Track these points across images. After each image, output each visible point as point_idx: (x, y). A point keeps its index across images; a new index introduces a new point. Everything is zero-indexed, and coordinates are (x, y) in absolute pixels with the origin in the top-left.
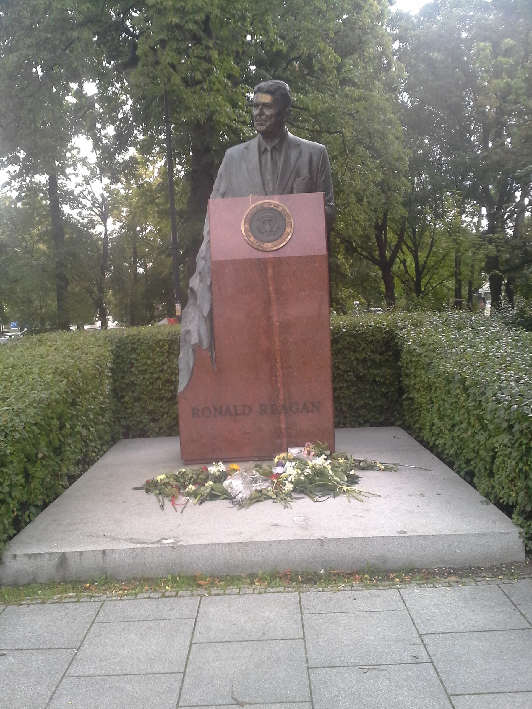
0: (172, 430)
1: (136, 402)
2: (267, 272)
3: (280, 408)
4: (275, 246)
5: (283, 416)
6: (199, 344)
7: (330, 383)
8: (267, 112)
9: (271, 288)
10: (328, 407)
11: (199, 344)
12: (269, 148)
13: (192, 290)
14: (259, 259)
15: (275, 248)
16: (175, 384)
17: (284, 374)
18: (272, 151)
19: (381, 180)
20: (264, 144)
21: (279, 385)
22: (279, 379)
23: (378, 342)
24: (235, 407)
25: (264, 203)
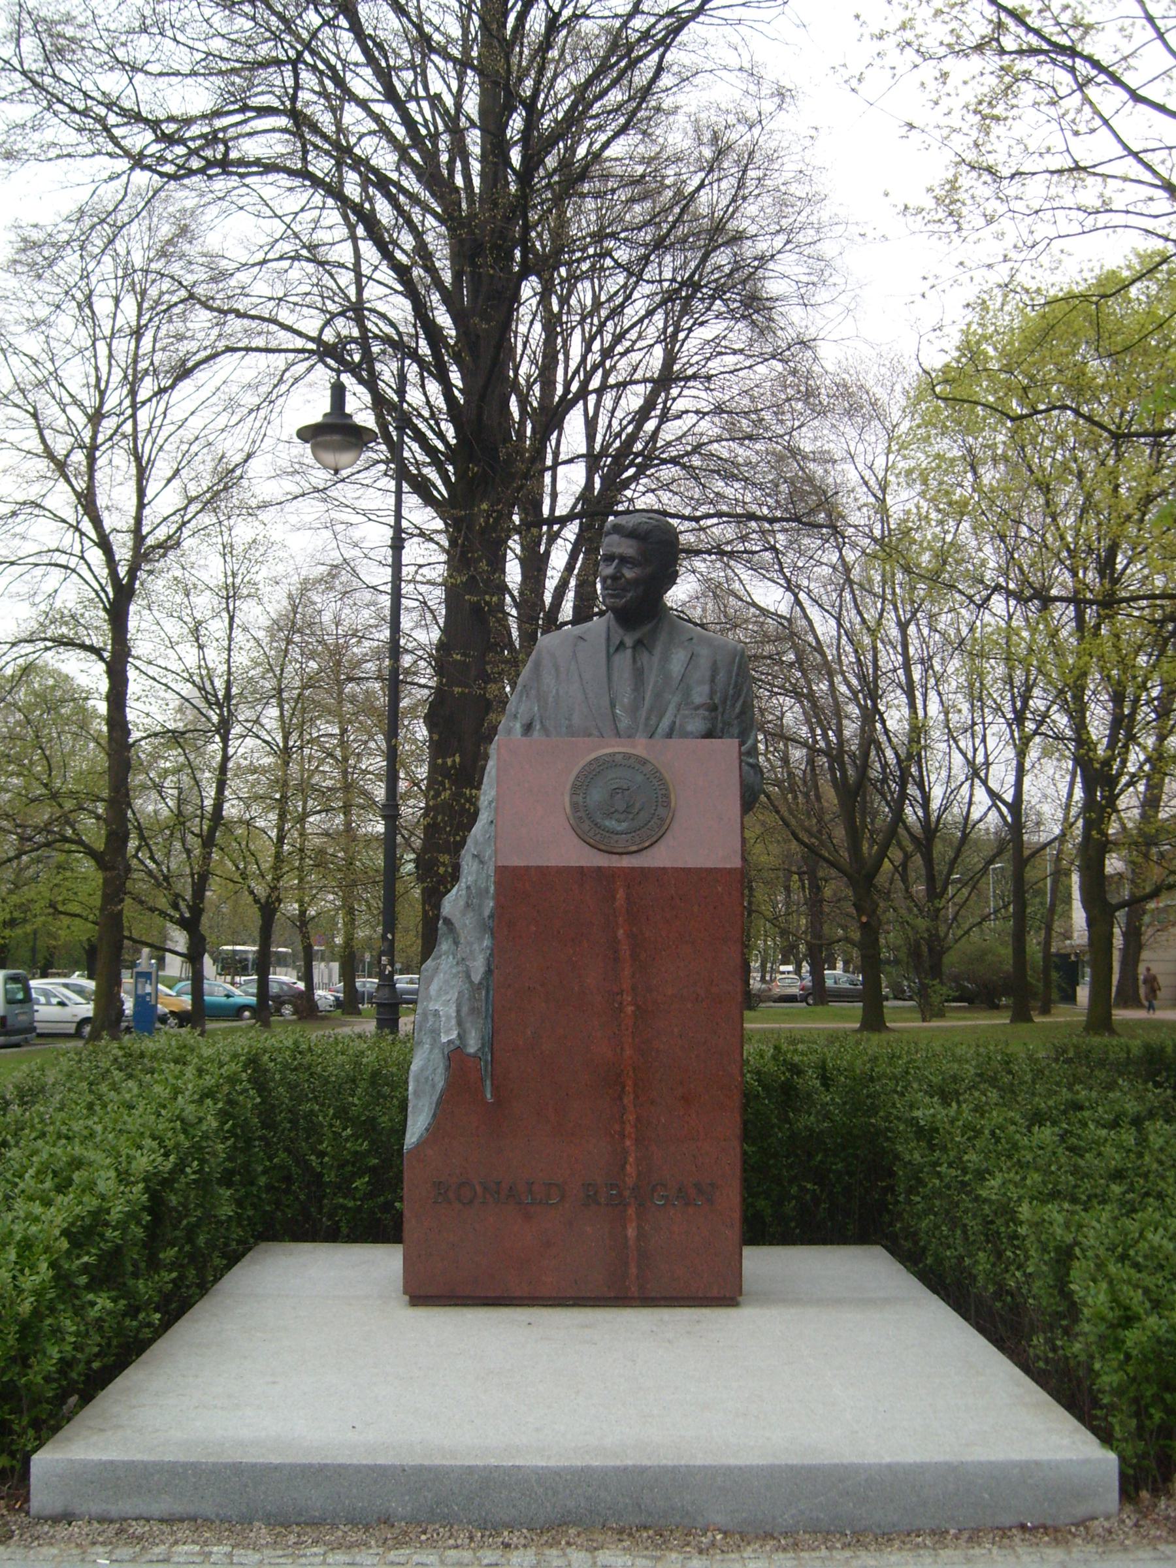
0: (377, 1227)
1: (301, 1171)
3: (627, 1193)
4: (633, 844)
6: (457, 1043)
7: (736, 1143)
8: (629, 574)
9: (621, 931)
10: (731, 1197)
11: (457, 1043)
12: (629, 641)
13: (448, 922)
14: (599, 869)
15: (634, 848)
16: (400, 1131)
17: (638, 1119)
18: (634, 648)
19: (51, 1273)
20: (618, 634)
22: (629, 1129)
23: (327, 1082)
25: (615, 754)
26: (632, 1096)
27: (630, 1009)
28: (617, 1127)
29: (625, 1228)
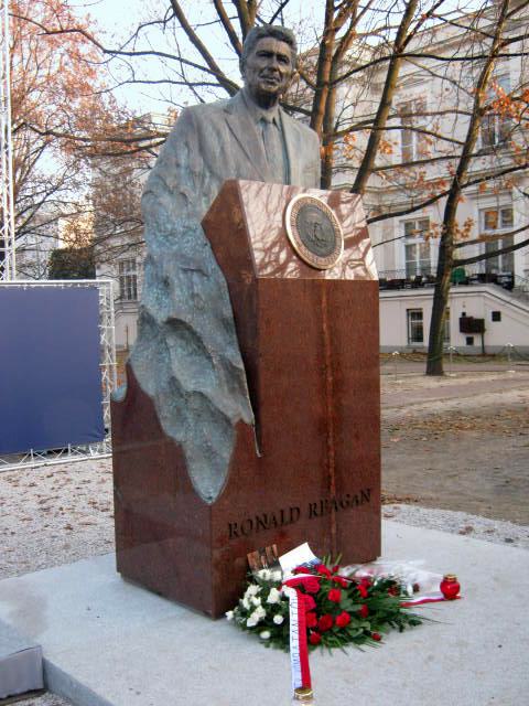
5: (333, 516)
9: (325, 326)
24: (282, 512)
27: (330, 379)
29: (330, 528)
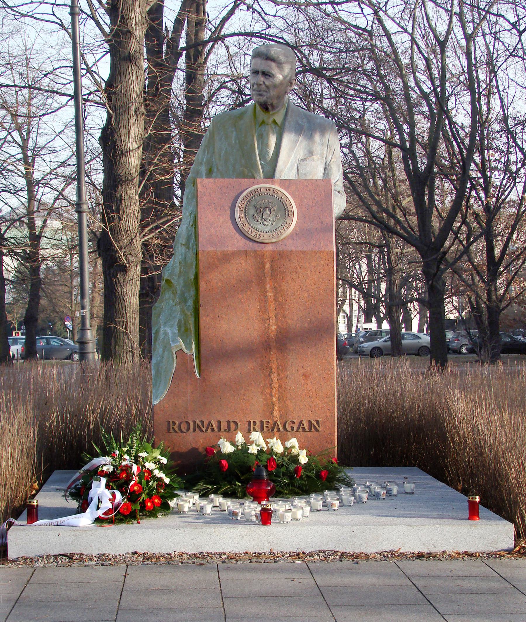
2: (264, 268)
17: (280, 386)
21: (274, 399)
26: (276, 374)
27: (274, 328)
28: (268, 391)
